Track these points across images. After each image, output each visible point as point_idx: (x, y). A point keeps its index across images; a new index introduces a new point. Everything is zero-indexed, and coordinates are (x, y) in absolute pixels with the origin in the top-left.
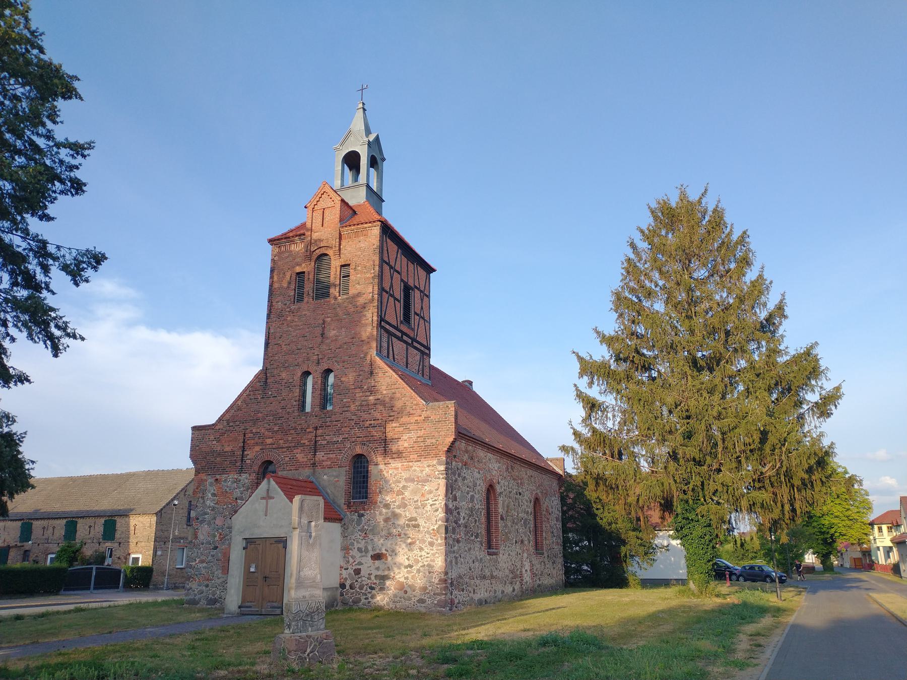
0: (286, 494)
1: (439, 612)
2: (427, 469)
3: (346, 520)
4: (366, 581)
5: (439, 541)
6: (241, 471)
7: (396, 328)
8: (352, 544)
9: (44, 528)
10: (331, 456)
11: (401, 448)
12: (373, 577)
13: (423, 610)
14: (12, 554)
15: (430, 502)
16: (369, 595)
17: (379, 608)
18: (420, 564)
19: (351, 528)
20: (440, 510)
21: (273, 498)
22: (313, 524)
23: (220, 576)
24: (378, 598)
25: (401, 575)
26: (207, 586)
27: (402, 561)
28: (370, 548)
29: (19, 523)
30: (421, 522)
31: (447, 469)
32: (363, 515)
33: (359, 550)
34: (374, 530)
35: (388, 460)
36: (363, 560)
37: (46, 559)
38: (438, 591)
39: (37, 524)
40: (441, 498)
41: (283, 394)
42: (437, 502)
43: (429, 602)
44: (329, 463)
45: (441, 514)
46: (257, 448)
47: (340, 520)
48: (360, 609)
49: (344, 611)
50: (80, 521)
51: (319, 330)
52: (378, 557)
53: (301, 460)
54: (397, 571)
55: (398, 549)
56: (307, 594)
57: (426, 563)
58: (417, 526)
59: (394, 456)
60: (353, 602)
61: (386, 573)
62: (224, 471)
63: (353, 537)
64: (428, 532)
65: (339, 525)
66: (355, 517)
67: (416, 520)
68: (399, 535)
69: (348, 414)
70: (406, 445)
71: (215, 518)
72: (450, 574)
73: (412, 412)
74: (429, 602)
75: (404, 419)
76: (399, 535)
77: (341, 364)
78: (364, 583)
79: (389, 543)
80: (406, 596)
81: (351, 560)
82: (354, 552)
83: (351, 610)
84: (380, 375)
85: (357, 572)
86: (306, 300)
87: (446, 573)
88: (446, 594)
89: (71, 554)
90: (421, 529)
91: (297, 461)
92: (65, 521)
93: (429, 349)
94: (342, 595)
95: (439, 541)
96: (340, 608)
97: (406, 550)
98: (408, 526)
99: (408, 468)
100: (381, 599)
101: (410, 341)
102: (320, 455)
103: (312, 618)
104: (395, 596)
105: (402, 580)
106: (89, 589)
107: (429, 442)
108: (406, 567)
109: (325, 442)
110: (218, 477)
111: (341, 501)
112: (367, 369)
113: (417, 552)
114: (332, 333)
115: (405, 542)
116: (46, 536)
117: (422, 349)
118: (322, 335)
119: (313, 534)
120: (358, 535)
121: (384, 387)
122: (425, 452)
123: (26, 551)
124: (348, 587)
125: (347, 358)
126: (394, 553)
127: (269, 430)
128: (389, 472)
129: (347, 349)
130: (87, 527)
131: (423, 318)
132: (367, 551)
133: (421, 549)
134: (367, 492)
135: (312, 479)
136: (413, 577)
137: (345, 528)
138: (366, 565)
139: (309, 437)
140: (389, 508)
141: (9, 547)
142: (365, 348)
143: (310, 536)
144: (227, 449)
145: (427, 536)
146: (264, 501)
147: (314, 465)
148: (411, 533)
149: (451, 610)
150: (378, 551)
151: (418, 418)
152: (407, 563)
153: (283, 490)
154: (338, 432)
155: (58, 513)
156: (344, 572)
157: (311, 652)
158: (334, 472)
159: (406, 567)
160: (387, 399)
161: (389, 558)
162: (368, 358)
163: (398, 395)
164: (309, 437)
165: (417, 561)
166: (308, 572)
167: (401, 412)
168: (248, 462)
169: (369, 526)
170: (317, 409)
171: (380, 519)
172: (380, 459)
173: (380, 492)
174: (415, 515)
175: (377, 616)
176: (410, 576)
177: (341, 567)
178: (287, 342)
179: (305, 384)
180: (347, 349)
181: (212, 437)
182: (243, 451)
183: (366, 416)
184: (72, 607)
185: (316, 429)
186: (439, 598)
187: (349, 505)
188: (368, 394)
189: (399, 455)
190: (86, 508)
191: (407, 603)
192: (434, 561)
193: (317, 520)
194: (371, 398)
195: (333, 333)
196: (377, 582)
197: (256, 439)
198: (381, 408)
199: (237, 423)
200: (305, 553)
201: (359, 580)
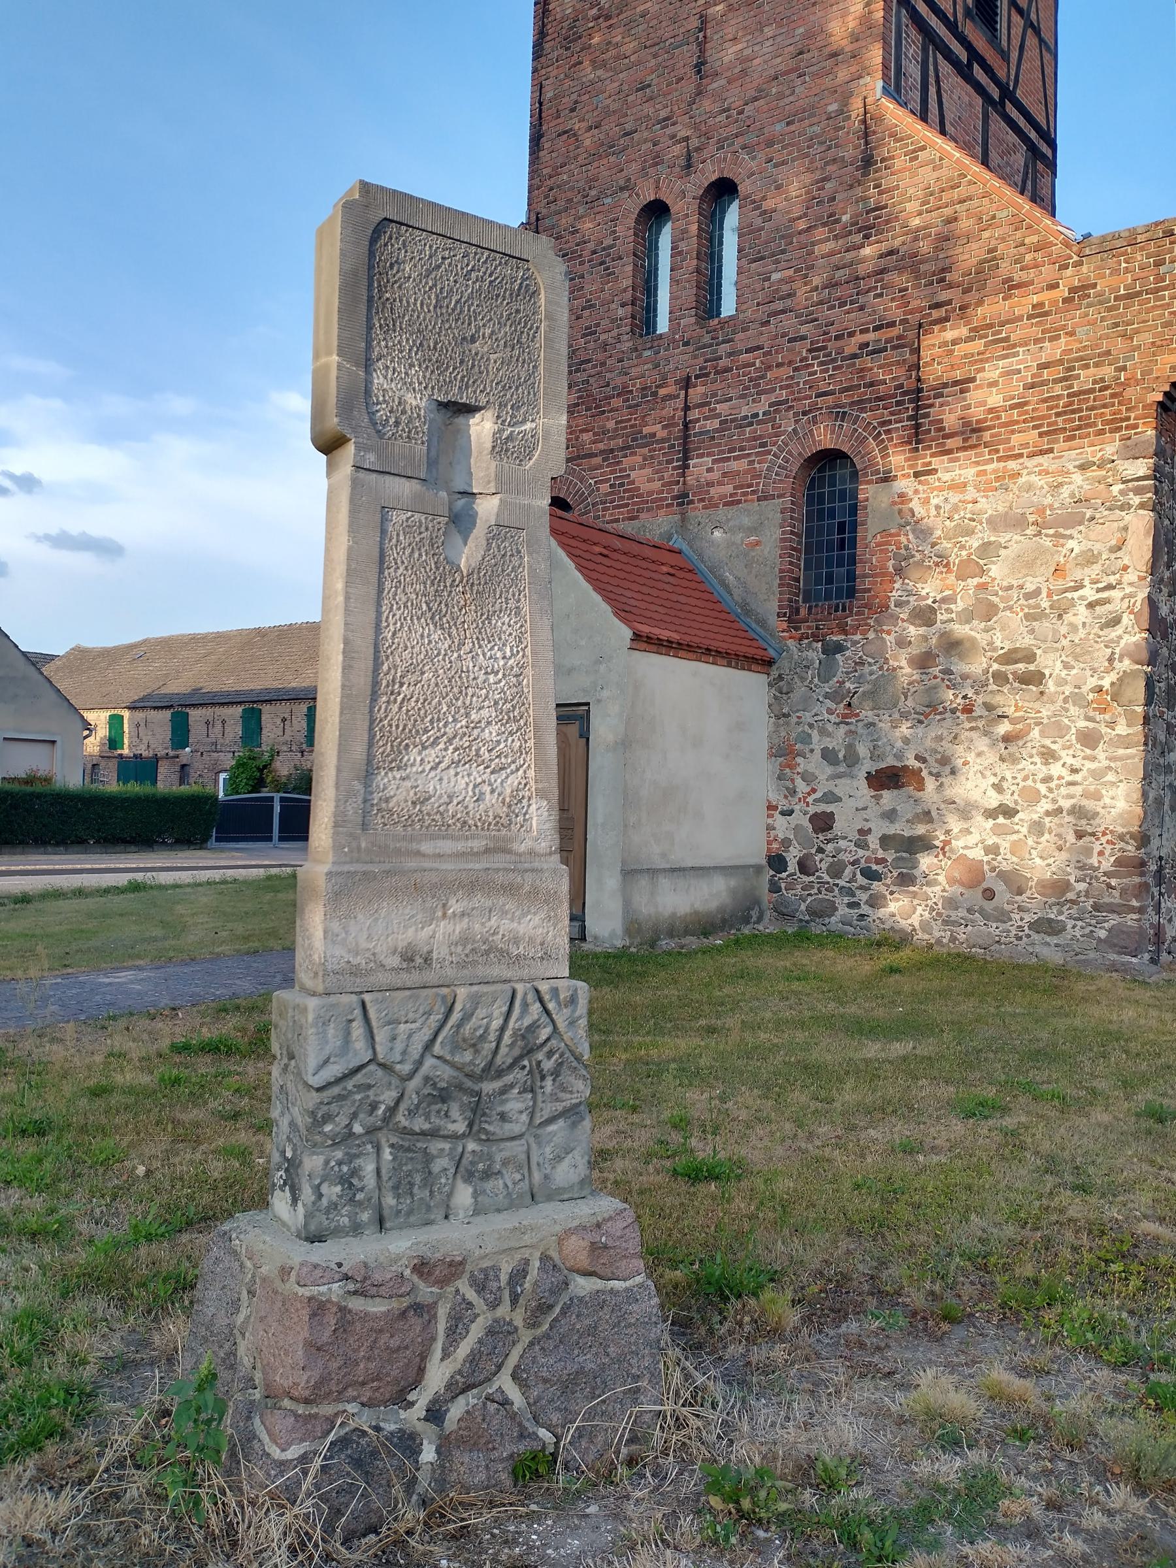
0: (581, 568)
1: (1113, 968)
2: (1077, 478)
3: (784, 665)
4: (848, 851)
5: (1122, 729)
7: (952, 27)
8: (806, 739)
9: (207, 723)
10: (734, 465)
11: (977, 413)
12: (873, 841)
13: (1055, 957)
14: (163, 770)
15: (1089, 593)
16: (863, 897)
17: (896, 940)
18: (1045, 805)
19: (800, 690)
20: (1127, 619)
22: (482, 428)
24: (893, 907)
25: (970, 840)
27: (975, 796)
28: (863, 750)
29: (167, 714)
30: (1050, 663)
31: (1158, 474)
32: (839, 648)
33: (829, 756)
34: (880, 692)
35: (927, 458)
36: (842, 787)
37: (216, 781)
38: (1115, 898)
39: (195, 714)
40: (1131, 576)
41: (588, 288)
42: (1116, 594)
43: (1074, 930)
44: (729, 489)
45: (1131, 635)
47: (766, 664)
48: (835, 939)
49: (778, 942)
50: (266, 709)
51: (689, 54)
52: (888, 779)
53: (645, 487)
54: (955, 824)
55: (960, 754)
56: (439, 934)
57: (1066, 804)
58: (1036, 678)
59: (950, 443)
60: (811, 911)
61: (921, 829)
63: (807, 717)
64: (1077, 698)
65: (762, 679)
66: (815, 654)
67: (1030, 658)
68: (968, 710)
69: (788, 323)
70: (995, 399)
72: (1155, 842)
73: (1019, 276)
74: (1074, 930)
75: (990, 309)
76: (968, 710)
78: (846, 857)
79: (928, 736)
80: (989, 906)
81: (802, 787)
82: (812, 763)
83: (802, 938)
84: (898, 163)
85: (823, 823)
87: (1143, 840)
88: (1141, 910)
89: (254, 772)
90: (1051, 686)
91: (634, 492)
92: (239, 710)
93: (1052, 145)
94: (774, 888)
95: (1122, 729)
96: (768, 927)
97: (991, 757)
98: (1000, 678)
99: (1004, 480)
100: (902, 910)
101: (995, 93)
102: (701, 467)
103: (477, 1111)
104: (951, 903)
105: (977, 854)
106: (270, 839)
107: (1085, 378)
108: (991, 814)
109: (716, 423)
111: (768, 604)
112: (850, 152)
113: (1033, 766)
114: (725, 55)
115: (986, 734)
116: (212, 738)
117: (1033, 135)
118: (699, 67)
119: (487, 508)
120: (824, 710)
121: (912, 206)
122: (1069, 415)
123: (183, 766)
124: (792, 866)
125: (779, 127)
126: (947, 766)
128: (933, 499)
129: (781, 96)
130: (279, 721)
131: (1037, 31)
132: (852, 759)
133: (1049, 756)
134: (852, 577)
135: (678, 543)
136: (1015, 848)
137: (781, 689)
138: (851, 804)
139: (668, 411)
140: (930, 623)
141: (156, 759)
142: (842, 74)
143: (460, 522)
145: (1074, 710)
148: (1009, 701)
149: (1154, 961)
150: (890, 761)
151: (1046, 296)
152: (993, 800)
153: (571, 555)
154: (755, 387)
155: (228, 694)
156: (780, 822)
157: (456, 1389)
158: (743, 516)
159: (991, 814)
160: (925, 247)
161: (930, 784)
162: (856, 106)
163: (965, 224)
164: (668, 411)
165: (1033, 797)
166: (433, 777)
167: (979, 281)
169: (860, 680)
170: (689, 320)
171: (903, 665)
172: (897, 459)
173: (899, 571)
174: (1027, 641)
175: (893, 970)
176: (1005, 844)
177: (771, 807)
178: (591, 118)
179: (652, 249)
180: (781, 96)
183: (853, 319)
184: (122, 879)
185: (686, 384)
186: (1114, 920)
187: (792, 617)
188: (857, 238)
189: (972, 434)
190: (277, 685)
191: (994, 928)
192: (1097, 797)
193: (514, 407)
194: (867, 251)
195: (730, 53)
196: (890, 856)
198: (900, 279)
200: (414, 639)
201: (829, 848)
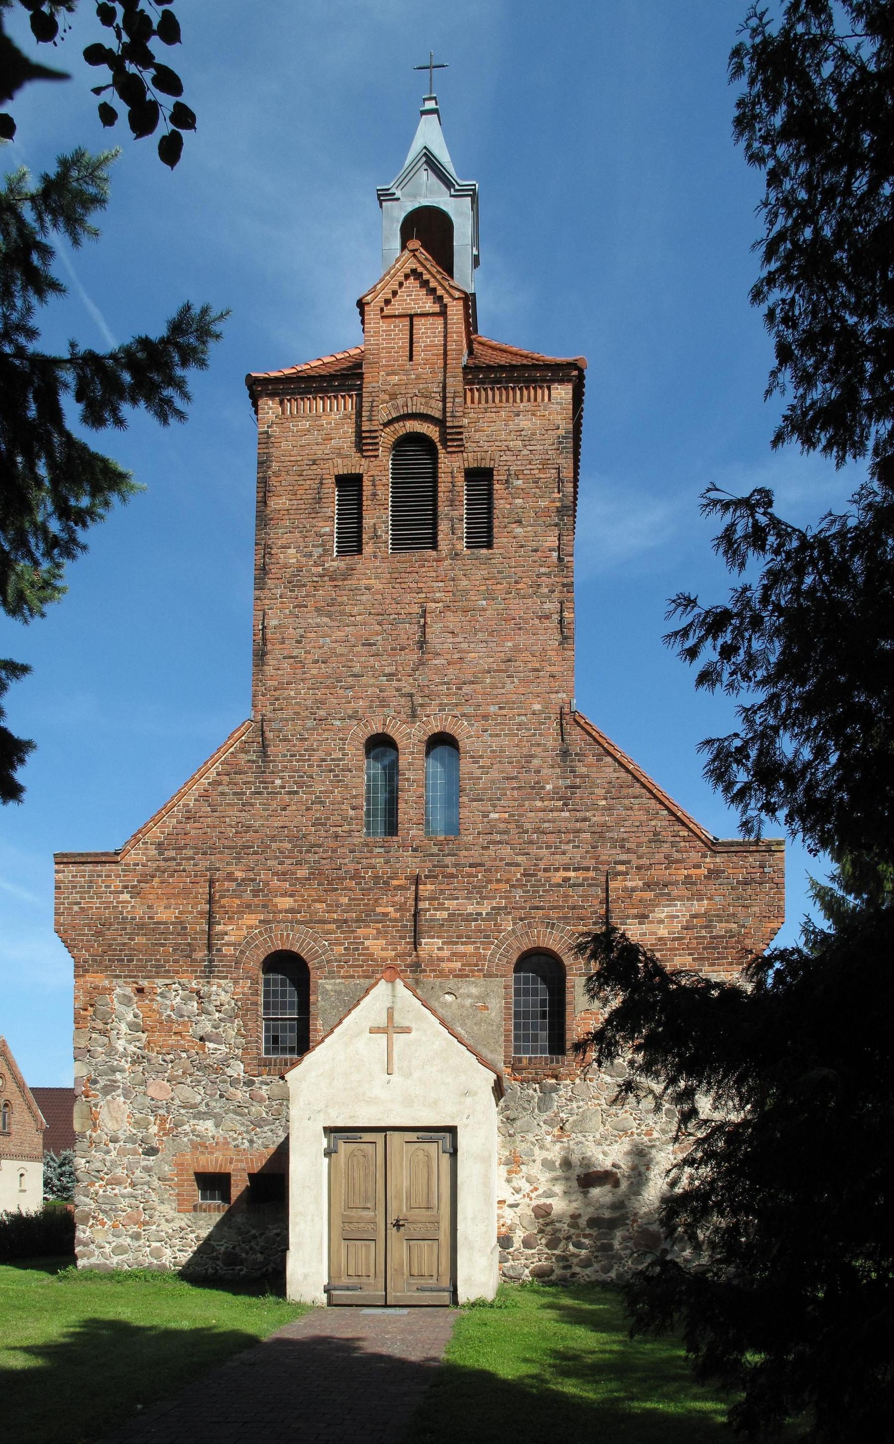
6: (209, 972)
10: (461, 948)
21: (407, 1030)
23: (172, 1214)
26: (136, 1237)
46: (251, 919)
53: (378, 953)
62: (159, 971)
70: (663, 932)
71: (144, 1083)
77: (478, 725)
86: (368, 549)
102: (431, 945)
107: (720, 928)
110: (144, 983)
125: (493, 709)
127: (282, 875)
129: (493, 686)
144: (164, 914)
146: (382, 1038)
147: (416, 967)
154: (478, 892)
158: (472, 989)
168: (227, 951)
181: (117, 884)
182: (211, 923)
197: (248, 895)
199: (189, 852)
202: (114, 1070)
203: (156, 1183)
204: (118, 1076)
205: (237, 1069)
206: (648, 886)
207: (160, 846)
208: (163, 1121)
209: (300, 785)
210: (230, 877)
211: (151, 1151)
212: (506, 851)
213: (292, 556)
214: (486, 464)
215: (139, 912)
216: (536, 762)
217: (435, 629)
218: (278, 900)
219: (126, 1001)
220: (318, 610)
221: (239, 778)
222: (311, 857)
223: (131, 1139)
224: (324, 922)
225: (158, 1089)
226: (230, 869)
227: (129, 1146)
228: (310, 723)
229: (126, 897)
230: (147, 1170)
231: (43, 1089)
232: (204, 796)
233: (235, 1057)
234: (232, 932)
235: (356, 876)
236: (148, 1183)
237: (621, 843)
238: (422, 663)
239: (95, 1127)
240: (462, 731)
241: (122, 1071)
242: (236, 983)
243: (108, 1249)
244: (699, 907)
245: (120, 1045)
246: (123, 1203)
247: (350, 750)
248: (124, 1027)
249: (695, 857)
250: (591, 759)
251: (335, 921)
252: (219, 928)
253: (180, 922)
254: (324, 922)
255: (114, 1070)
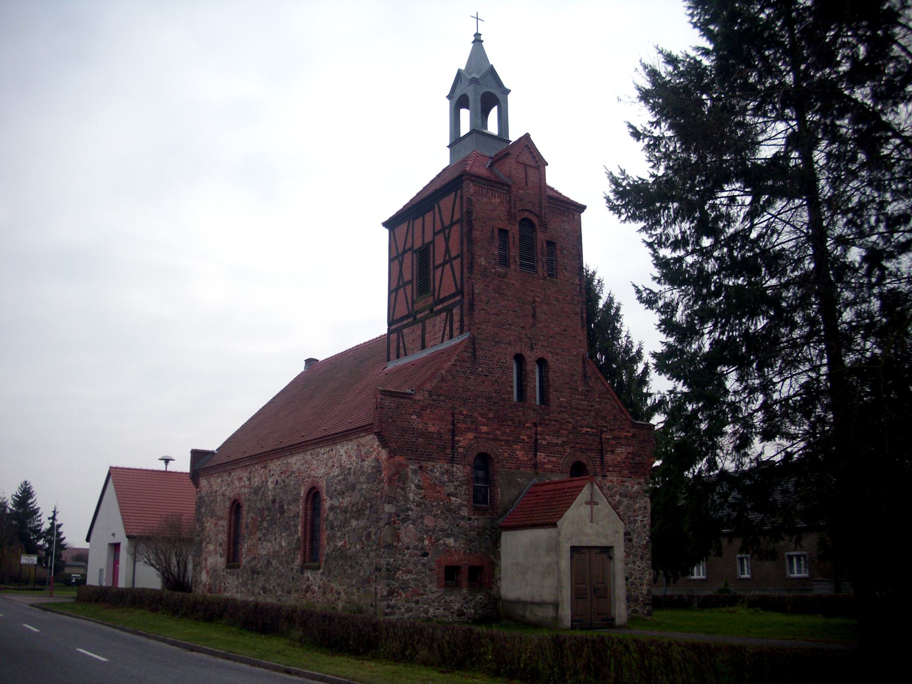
6: (452, 461)
10: (552, 459)
46: (470, 435)
62: (430, 458)
71: (422, 517)
102: (541, 456)
107: (637, 460)
110: (423, 464)
125: (560, 351)
144: (432, 429)
146: (589, 507)
168: (461, 450)
182: (453, 436)
197: (469, 424)
199: (443, 398)
202: (408, 509)
203: (428, 572)
204: (410, 513)
205: (464, 512)
206: (614, 438)
207: (430, 393)
208: (431, 538)
209: (490, 372)
210: (461, 413)
211: (426, 554)
212: (566, 416)
213: (483, 261)
214: (554, 240)
215: (420, 426)
216: (575, 378)
217: (538, 310)
218: (481, 427)
219: (415, 472)
220: (494, 289)
221: (464, 364)
222: (495, 408)
223: (416, 548)
224: (500, 440)
225: (429, 522)
226: (461, 409)
227: (415, 552)
228: (492, 343)
229: (414, 417)
230: (424, 565)
231: (444, 170)
232: (449, 371)
233: (464, 505)
234: (463, 440)
235: (512, 420)
236: (424, 572)
237: (604, 418)
238: (534, 324)
239: (399, 540)
240: (550, 358)
241: (412, 510)
242: (464, 467)
243: (403, 610)
244: (630, 449)
245: (411, 496)
246: (412, 584)
247: (508, 359)
248: (413, 486)
249: (627, 428)
250: (593, 380)
251: (504, 440)
252: (457, 438)
253: (439, 433)
254: (500, 440)
255: (408, 509)
